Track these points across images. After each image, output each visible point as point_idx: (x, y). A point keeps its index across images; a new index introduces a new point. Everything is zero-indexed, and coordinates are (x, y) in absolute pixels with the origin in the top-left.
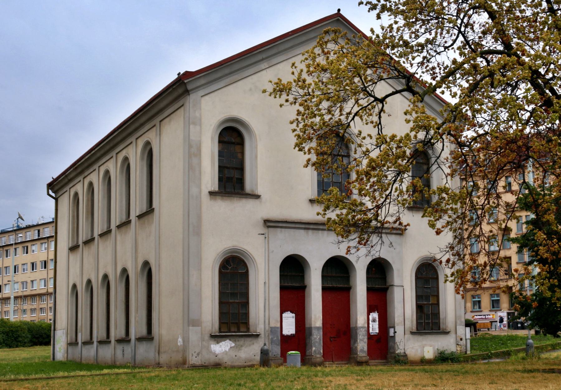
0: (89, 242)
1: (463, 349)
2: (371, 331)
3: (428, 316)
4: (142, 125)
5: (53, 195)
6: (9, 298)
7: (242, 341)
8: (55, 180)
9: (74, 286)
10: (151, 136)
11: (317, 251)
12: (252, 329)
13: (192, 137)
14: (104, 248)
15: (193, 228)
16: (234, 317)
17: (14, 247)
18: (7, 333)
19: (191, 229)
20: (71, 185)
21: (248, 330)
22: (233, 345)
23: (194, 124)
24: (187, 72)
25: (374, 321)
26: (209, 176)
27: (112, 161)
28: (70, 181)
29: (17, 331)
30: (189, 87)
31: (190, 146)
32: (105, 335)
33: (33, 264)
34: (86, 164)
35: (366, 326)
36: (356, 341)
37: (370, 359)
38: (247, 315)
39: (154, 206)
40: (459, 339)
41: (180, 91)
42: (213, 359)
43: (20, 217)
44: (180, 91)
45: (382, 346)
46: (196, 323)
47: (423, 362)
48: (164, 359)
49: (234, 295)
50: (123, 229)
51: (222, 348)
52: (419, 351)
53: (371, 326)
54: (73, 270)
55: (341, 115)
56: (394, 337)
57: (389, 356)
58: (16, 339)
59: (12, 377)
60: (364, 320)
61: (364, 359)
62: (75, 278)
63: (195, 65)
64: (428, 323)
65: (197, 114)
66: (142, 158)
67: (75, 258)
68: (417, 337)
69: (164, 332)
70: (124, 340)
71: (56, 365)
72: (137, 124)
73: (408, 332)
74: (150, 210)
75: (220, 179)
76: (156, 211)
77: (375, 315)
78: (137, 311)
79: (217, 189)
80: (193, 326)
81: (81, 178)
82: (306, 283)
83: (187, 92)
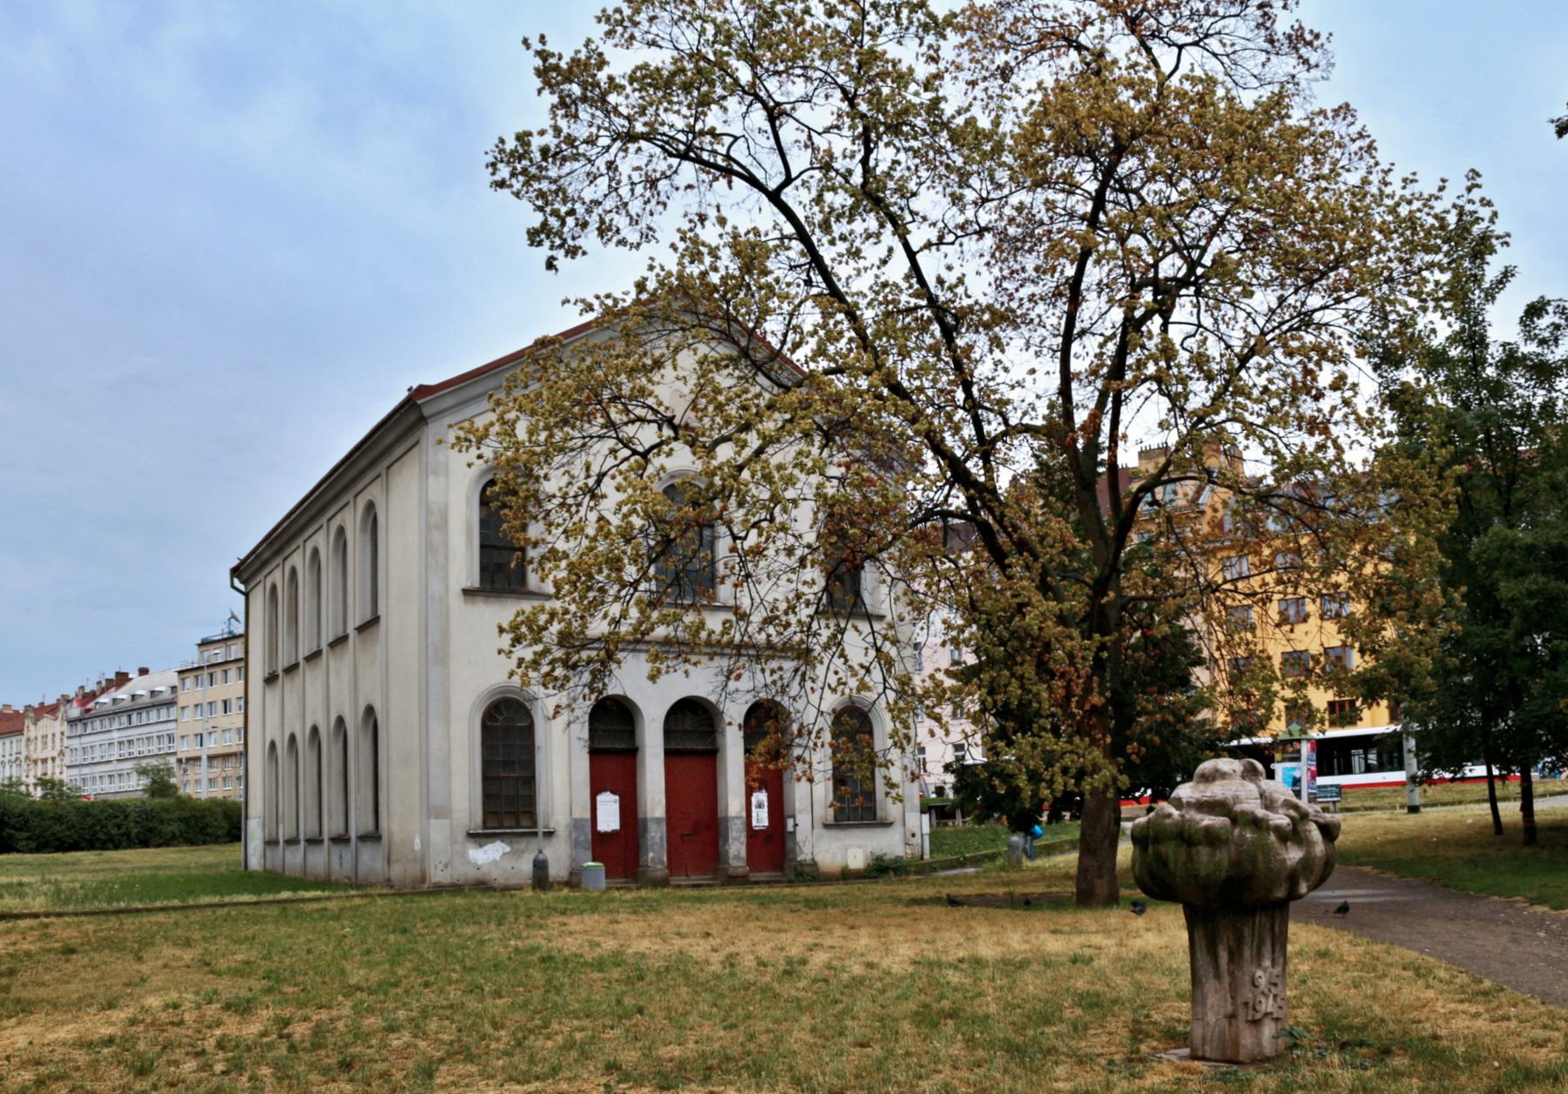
0: (291, 669)
1: (917, 851)
2: (754, 823)
4: (362, 473)
5: (242, 587)
6: (198, 759)
7: (522, 843)
8: (243, 562)
9: (273, 745)
10: (374, 492)
11: (653, 694)
13: (432, 497)
14: (312, 679)
15: (436, 652)
16: (508, 798)
17: (206, 672)
19: (431, 654)
20: (266, 571)
21: (534, 824)
22: (508, 849)
23: (436, 473)
24: (421, 387)
25: (760, 806)
26: (464, 565)
27: (324, 530)
28: (265, 563)
29: (204, 817)
30: (427, 411)
31: (428, 512)
32: (317, 829)
33: (225, 702)
34: (285, 537)
35: (744, 814)
36: (727, 840)
38: (531, 800)
39: (381, 611)
41: (412, 417)
42: (472, 874)
43: (233, 617)
44: (412, 417)
45: (773, 846)
46: (442, 812)
47: (846, 875)
48: (396, 872)
49: (508, 764)
50: (338, 649)
51: (490, 857)
53: (754, 815)
54: (274, 716)
55: (588, 476)
56: (794, 833)
57: (786, 865)
58: (202, 830)
59: (122, 905)
60: (738, 801)
61: (741, 871)
62: (273, 732)
63: (433, 380)
64: (856, 809)
65: (441, 458)
66: (363, 529)
67: (273, 695)
68: (834, 833)
69: (395, 827)
70: (341, 840)
71: (244, 879)
72: (354, 472)
74: (375, 621)
75: (483, 569)
76: (383, 620)
77: (761, 797)
78: (358, 790)
79: (477, 584)
81: (279, 560)
82: (638, 743)
83: (422, 420)
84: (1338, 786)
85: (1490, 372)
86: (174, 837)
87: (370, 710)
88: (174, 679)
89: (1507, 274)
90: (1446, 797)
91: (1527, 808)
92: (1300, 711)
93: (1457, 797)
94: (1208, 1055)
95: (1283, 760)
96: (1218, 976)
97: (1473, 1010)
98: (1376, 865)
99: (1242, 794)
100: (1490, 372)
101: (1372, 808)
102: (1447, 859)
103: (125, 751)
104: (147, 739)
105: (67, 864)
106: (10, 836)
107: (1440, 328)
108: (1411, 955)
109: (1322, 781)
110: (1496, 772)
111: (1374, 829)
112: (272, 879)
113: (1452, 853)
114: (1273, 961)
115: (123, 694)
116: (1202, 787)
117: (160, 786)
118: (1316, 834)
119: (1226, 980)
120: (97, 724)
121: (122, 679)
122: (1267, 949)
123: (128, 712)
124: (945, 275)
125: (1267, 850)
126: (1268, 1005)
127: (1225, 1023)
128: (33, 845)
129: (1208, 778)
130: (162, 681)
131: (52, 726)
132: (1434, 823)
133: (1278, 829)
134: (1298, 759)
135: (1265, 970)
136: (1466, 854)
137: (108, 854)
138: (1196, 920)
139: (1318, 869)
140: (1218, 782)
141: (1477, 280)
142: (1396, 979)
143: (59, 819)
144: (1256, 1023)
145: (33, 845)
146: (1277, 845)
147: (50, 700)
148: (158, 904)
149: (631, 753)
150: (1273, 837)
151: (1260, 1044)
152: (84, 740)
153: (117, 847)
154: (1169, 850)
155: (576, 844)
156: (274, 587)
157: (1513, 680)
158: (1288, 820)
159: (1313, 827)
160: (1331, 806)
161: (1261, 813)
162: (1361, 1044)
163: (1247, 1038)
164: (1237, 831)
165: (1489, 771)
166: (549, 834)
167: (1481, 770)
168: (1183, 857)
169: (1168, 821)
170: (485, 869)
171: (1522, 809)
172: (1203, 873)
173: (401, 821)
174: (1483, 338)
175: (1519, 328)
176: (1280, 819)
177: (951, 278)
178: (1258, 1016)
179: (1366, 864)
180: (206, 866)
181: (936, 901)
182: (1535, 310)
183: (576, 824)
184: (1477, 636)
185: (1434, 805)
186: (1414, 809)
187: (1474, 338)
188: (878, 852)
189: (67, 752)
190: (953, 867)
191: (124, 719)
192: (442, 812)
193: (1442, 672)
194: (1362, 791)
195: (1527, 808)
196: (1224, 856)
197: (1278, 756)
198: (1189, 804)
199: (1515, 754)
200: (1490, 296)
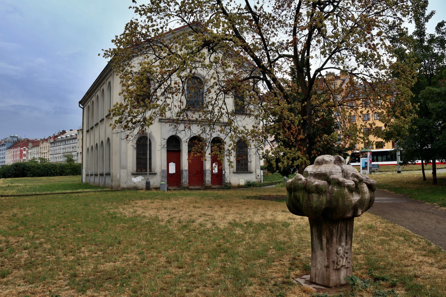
0: (92, 128)
1: (259, 180)
3: (242, 164)
5: (82, 107)
9: (88, 148)
12: (153, 170)
16: (143, 164)
18: (72, 169)
22: (143, 178)
27: (99, 91)
28: (87, 100)
37: (212, 185)
40: (257, 176)
42: (133, 185)
45: (219, 178)
46: (125, 167)
48: (114, 184)
51: (138, 180)
52: (237, 182)
56: (225, 174)
58: (76, 171)
61: (209, 185)
62: (88, 146)
68: (236, 175)
69: (113, 172)
73: (231, 172)
78: (105, 161)
80: (123, 169)
81: (90, 99)
84: (378, 165)
85: (426, 44)
86: (68, 173)
87: (108, 139)
88: (76, 132)
89: (432, 13)
90: (408, 169)
91: (434, 173)
92: (368, 144)
93: (411, 169)
94: (317, 282)
95: (362, 157)
96: (322, 249)
97: (430, 261)
98: (389, 189)
99: (334, 171)
100: (426, 44)
101: (387, 171)
102: (410, 188)
103: (64, 151)
104: (67, 148)
105: (38, 180)
106: (26, 173)
107: (410, 27)
108: (402, 229)
109: (373, 163)
110: (424, 162)
111: (388, 177)
112: (87, 186)
113: (411, 186)
114: (346, 243)
115: (64, 136)
116: (317, 167)
117: (70, 160)
118: (366, 189)
119: (325, 251)
120: (57, 144)
121: (64, 132)
122: (344, 238)
123: (65, 141)
124: (257, 5)
125: (343, 196)
126: (343, 262)
127: (324, 269)
128: (32, 175)
129: (320, 163)
130: (74, 133)
131: (47, 144)
132: (405, 177)
133: (348, 187)
134: (367, 157)
135: (342, 247)
136: (416, 186)
137: (52, 178)
138: (312, 223)
139: (367, 203)
140: (323, 165)
141: (423, 15)
142: (397, 241)
143: (38, 168)
144: (338, 270)
145: (32, 175)
146: (348, 194)
147: (46, 138)
148: (44, 193)
149: (179, 152)
150: (346, 190)
151: (339, 279)
152: (54, 148)
153: (53, 176)
154: (300, 194)
155: (162, 177)
156: (89, 106)
157: (431, 135)
158: (353, 183)
159: (365, 185)
160: (376, 170)
161: (341, 179)
162: (383, 279)
163: (334, 277)
164: (330, 187)
165: (422, 162)
166: (155, 174)
167: (420, 162)
168: (306, 198)
169: (300, 182)
170: (136, 184)
171: (433, 173)
172: (315, 206)
173: (115, 171)
174: (424, 33)
175: (435, 30)
176: (350, 182)
177: (259, 6)
178: (339, 267)
179: (385, 189)
180: (74, 181)
181: (256, 198)
182: (441, 25)
183: (163, 171)
184: (421, 121)
185: (404, 171)
186: (399, 172)
187: (420, 32)
188: (249, 181)
189: (50, 151)
190: (269, 185)
191: (64, 142)
192: (125, 167)
193: (411, 131)
194: (384, 166)
195: (434, 173)
196: (324, 199)
197: (361, 156)
198: (311, 174)
199: (428, 156)
200: (427, 20)
